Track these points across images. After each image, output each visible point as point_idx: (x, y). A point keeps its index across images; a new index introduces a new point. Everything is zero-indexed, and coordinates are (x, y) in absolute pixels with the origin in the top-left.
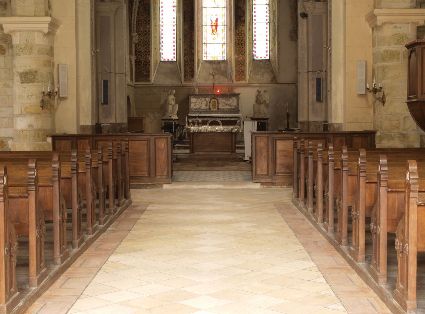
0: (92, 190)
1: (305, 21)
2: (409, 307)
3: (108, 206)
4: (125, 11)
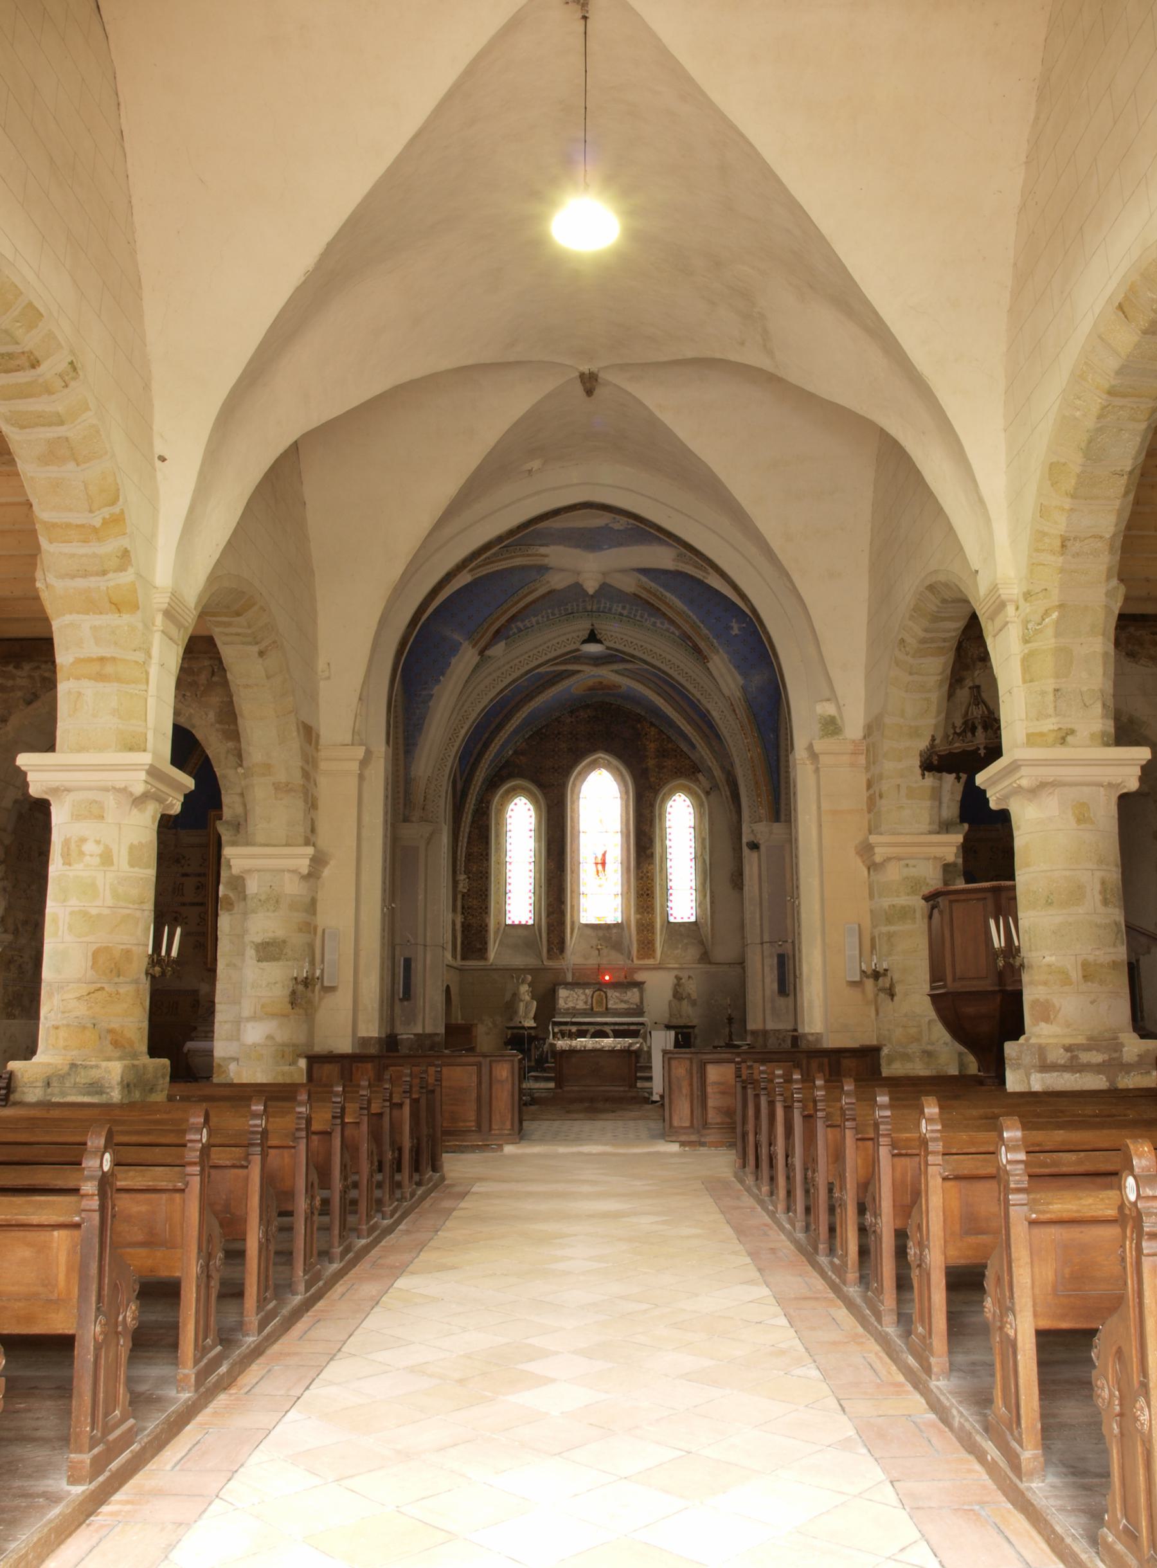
0: (371, 1154)
1: (755, 855)
2: (935, 1369)
3: (399, 1185)
4: (445, 839)
